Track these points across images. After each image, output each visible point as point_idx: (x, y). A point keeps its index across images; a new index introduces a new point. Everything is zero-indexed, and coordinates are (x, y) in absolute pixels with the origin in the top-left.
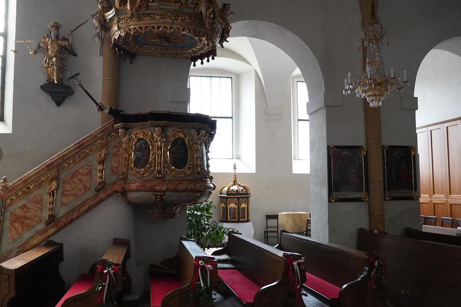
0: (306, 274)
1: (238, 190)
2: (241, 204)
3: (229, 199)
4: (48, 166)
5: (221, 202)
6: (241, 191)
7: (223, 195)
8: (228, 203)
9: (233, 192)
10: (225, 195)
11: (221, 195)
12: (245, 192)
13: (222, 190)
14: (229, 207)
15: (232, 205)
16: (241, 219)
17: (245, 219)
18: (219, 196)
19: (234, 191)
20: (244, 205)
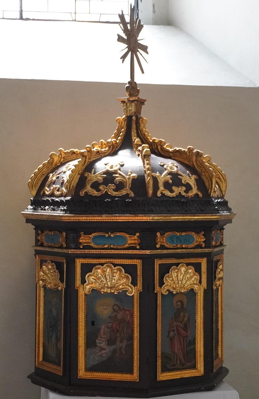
0: (61, 369)
1: (148, 179)
2: (165, 270)
3: (84, 240)
4: (45, 286)
5: (42, 254)
6: (167, 185)
7: (48, 212)
8: (79, 262)
9: (110, 189)
10: (59, 213)
11: (40, 212)
12: (195, 191)
13: (47, 177)
14: (84, 290)
15: (107, 278)
16: (165, 370)
17: (194, 367)
18: (29, 220)
19: (120, 186)
20: (182, 278)
